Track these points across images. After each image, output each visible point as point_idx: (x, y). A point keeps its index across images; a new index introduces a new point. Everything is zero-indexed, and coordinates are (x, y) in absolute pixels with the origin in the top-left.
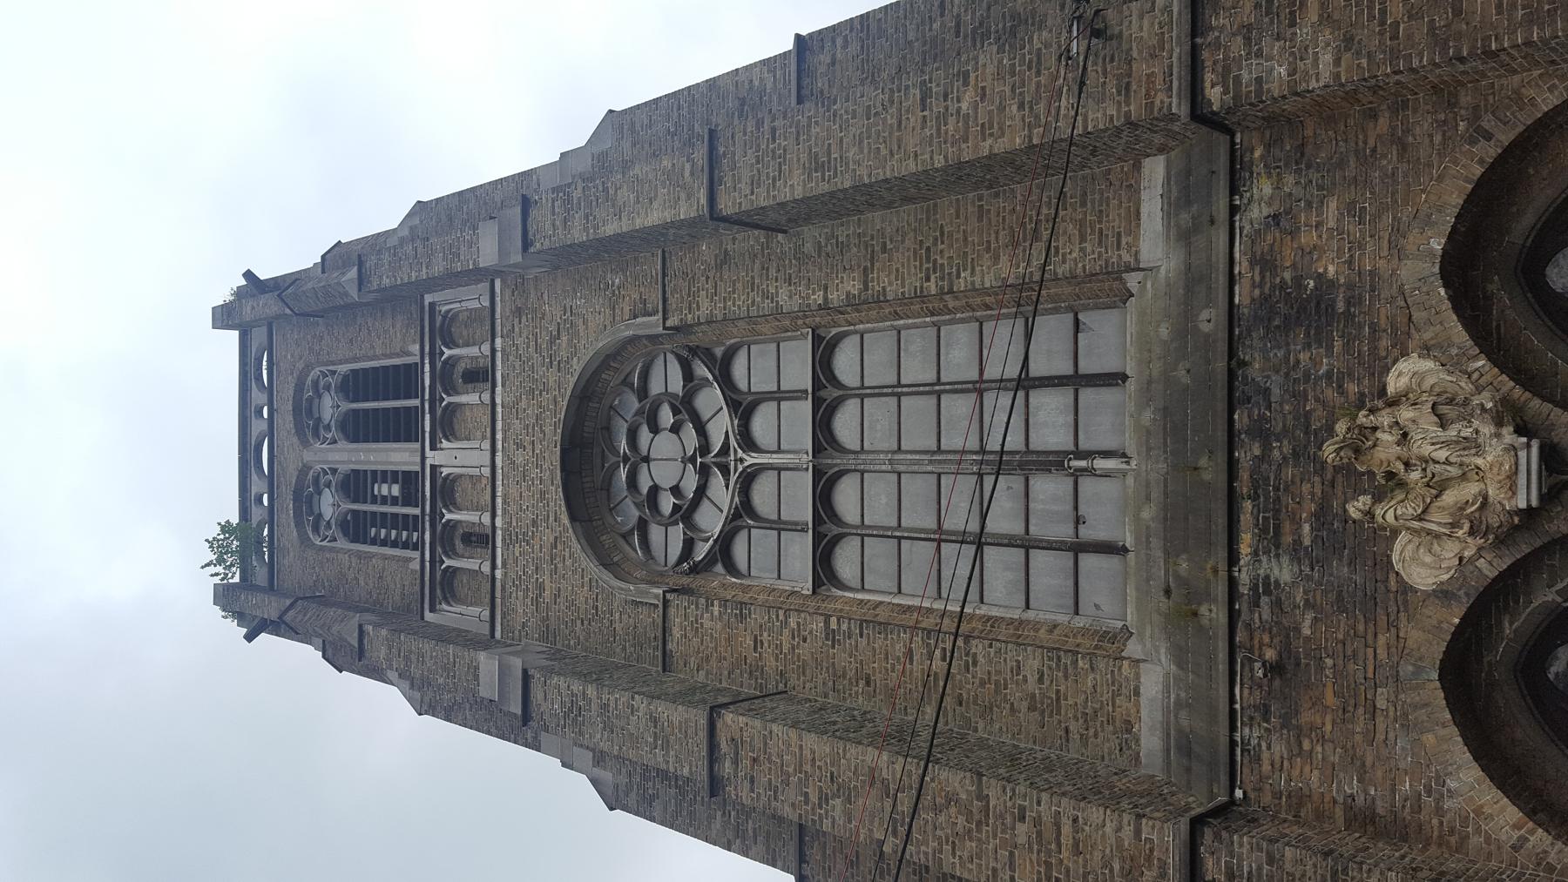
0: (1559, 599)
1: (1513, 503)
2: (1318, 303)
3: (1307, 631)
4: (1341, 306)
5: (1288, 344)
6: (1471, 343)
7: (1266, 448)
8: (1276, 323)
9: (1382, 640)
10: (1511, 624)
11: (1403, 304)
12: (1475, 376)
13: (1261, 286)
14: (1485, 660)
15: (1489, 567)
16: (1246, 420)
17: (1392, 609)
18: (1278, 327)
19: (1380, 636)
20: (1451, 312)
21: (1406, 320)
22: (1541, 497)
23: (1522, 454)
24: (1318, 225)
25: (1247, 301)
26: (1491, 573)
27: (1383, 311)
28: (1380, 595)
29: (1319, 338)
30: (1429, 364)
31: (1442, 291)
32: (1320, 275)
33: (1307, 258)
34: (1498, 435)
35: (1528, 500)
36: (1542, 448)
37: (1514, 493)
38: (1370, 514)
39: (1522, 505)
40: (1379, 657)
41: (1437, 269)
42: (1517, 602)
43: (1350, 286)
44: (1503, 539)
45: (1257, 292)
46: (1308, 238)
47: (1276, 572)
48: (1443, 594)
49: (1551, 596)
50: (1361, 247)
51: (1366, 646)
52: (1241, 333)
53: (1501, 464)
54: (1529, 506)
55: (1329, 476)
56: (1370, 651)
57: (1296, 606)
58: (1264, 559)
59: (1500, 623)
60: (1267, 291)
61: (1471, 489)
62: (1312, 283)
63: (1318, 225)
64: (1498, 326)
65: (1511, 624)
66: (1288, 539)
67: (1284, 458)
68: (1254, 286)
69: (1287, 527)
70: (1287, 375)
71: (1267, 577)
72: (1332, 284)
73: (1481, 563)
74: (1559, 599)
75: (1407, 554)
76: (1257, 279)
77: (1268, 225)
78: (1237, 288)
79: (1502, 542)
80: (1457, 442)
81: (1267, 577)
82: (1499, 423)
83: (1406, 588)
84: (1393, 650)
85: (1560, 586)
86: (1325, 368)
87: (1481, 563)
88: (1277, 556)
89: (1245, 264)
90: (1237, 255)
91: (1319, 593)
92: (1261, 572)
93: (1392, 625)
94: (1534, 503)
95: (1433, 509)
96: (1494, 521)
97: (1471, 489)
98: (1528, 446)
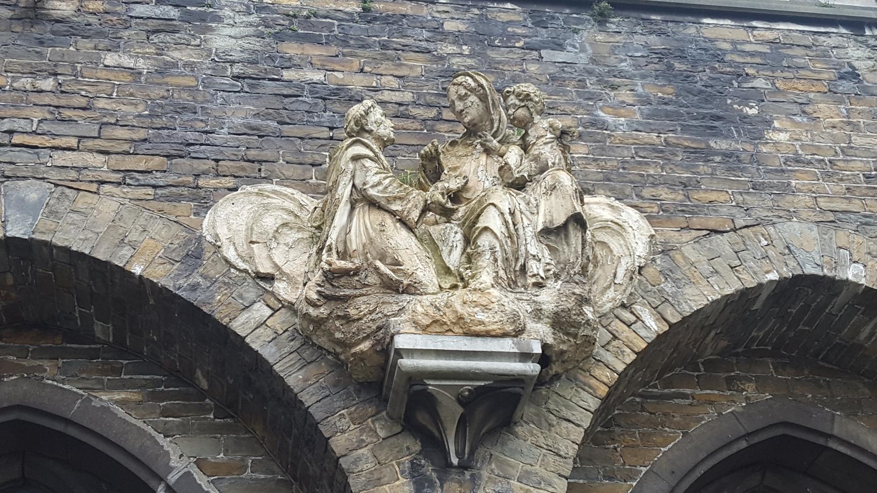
0: (172, 478)
1: (408, 328)
2: (719, 118)
3: (110, 59)
4: (719, 144)
5: (643, 77)
6: (687, 311)
7: (457, 38)
8: (677, 65)
9: (98, 160)
10: (122, 403)
11: (740, 223)
12: (627, 315)
13: (735, 51)
14: (47, 364)
15: (256, 325)
16: (505, 17)
17: (160, 179)
18: (670, 67)
19: (102, 158)
20: (738, 286)
21: (712, 224)
22: (417, 377)
23: (507, 345)
24: (855, 127)
25: (708, 33)
26: (240, 325)
27: (723, 197)
28: (182, 162)
29: (659, 114)
30: (641, 249)
31: (773, 276)
32: (769, 123)
33: (796, 109)
34: (537, 314)
35: (412, 352)
36: (518, 379)
37: (425, 329)
38: (361, 129)
39: (401, 342)
40: (56, 154)
41: (810, 270)
42: (165, 413)
43: (756, 159)
44: (311, 335)
45: (726, 46)
46: (826, 110)
47: (229, 31)
48: (194, 252)
49: (178, 457)
50: (828, 176)
51: (81, 138)
52: (651, 22)
53: (485, 308)
54: (399, 353)
55: (415, 111)
56: (73, 142)
57: (160, 52)
58: (253, 18)
59: (123, 386)
60: (728, 58)
61: (426, 273)
62: (754, 111)
63: (855, 127)
64: (685, 396)
65: (122, 403)
66: (291, 49)
67: (441, 58)
68: (734, 43)
69: (314, 51)
70: (590, 73)
71: (219, 19)
72: (757, 137)
73: (261, 311)
74: (172, 478)
75: (277, 201)
76: (748, 48)
77: (838, 67)
78: (728, 22)
79: (307, 341)
80: (516, 252)
81: (219, 19)
82: (561, 322)
83: (204, 202)
84: (73, 174)
85: (201, 479)
86: (610, 119)
87: (261, 311)
88: (261, 36)
89: (770, 36)
90: (782, 26)
91: (190, 82)
92: (227, 12)
93: (125, 178)
94: (406, 363)
95: (377, 216)
96: (360, 307)
97: (426, 273)
98: (525, 356)
